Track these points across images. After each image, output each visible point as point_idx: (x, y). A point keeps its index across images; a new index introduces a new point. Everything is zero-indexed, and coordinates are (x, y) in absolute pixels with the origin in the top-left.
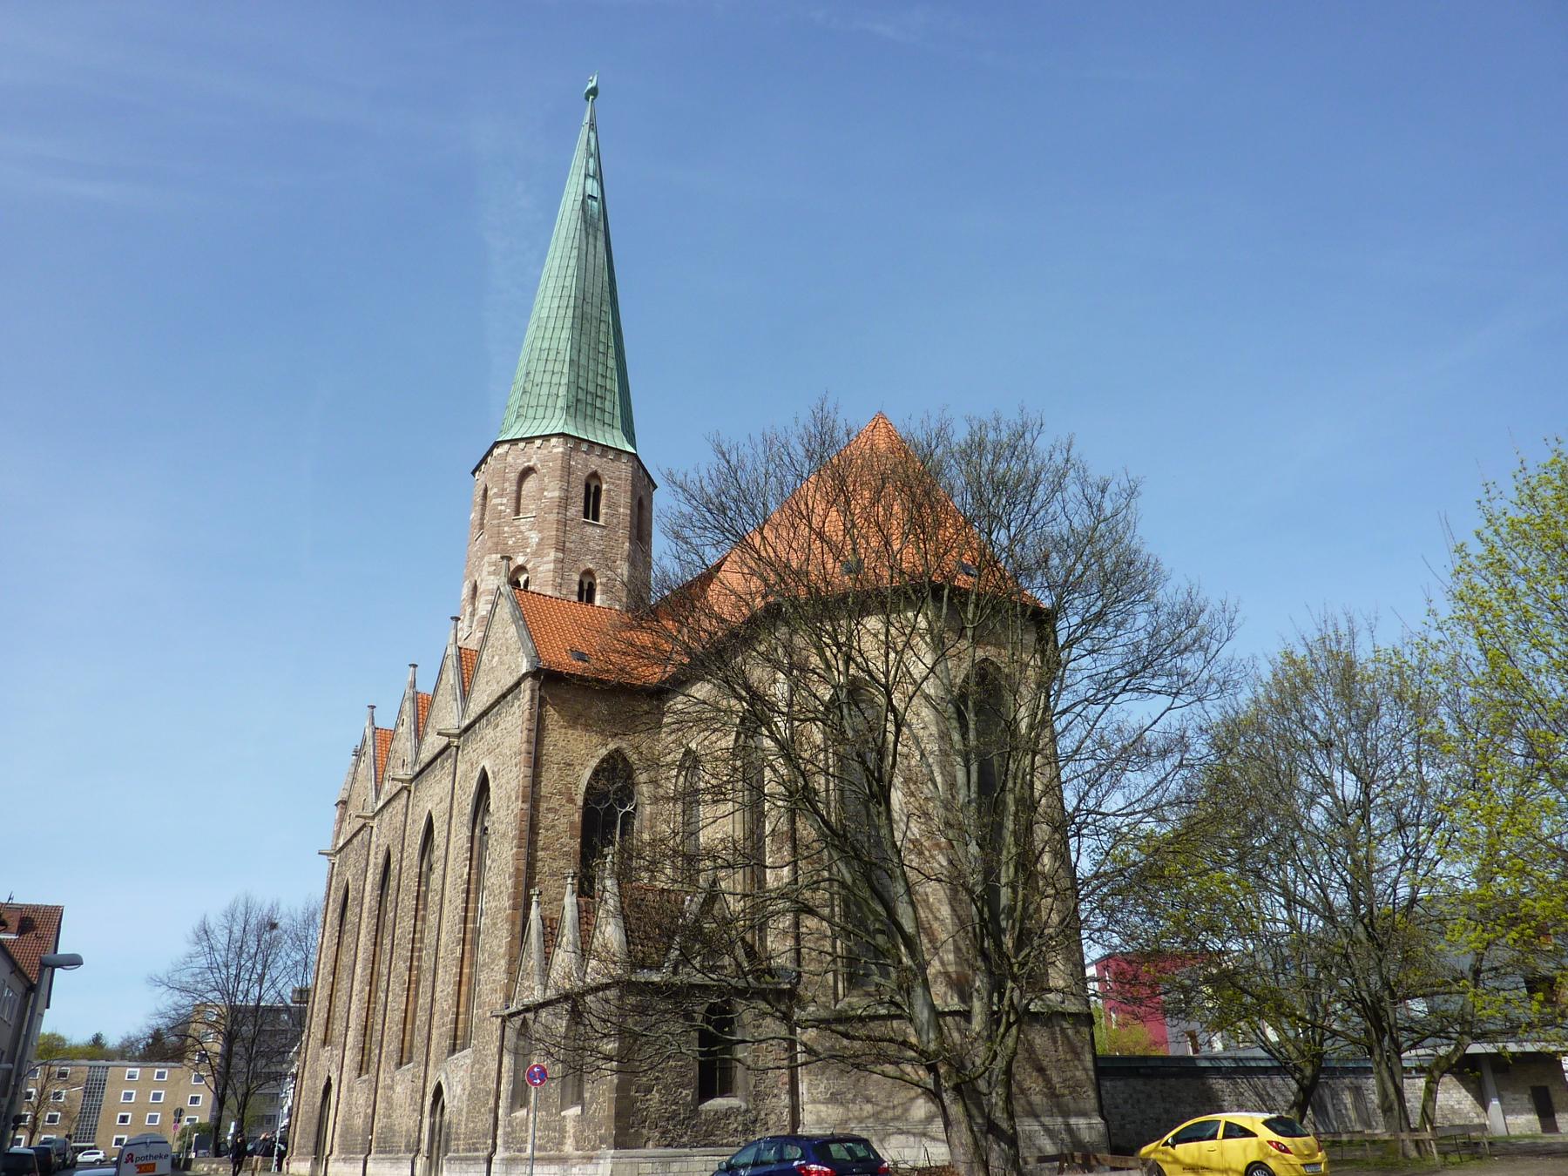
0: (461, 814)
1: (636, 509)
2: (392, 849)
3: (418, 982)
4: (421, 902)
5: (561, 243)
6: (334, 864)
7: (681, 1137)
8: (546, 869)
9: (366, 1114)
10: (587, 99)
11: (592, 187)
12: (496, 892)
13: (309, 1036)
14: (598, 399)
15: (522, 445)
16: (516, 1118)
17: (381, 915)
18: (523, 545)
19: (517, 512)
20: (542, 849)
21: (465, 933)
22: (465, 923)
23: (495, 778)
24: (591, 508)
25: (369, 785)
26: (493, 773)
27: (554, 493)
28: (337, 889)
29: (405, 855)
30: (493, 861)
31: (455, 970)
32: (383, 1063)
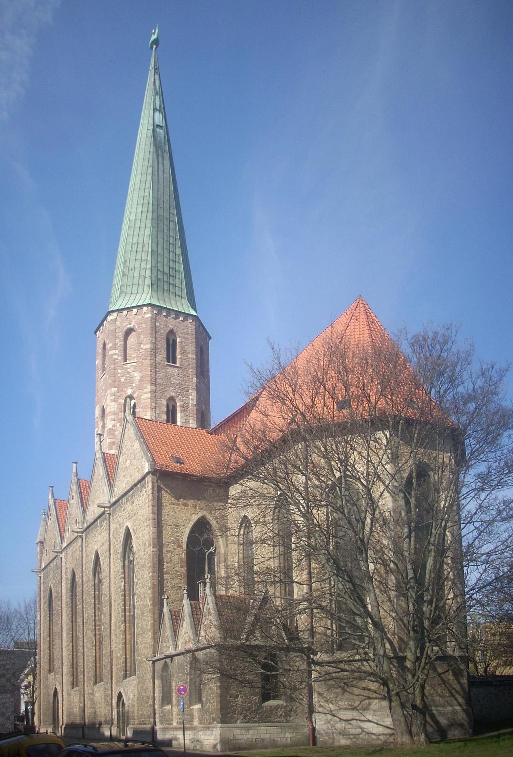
0: (116, 552)
1: (199, 355)
2: (75, 571)
3: (101, 643)
4: (97, 600)
5: (141, 164)
6: (40, 577)
7: (254, 718)
8: (169, 584)
9: (80, 707)
10: (152, 48)
11: (159, 118)
12: (142, 597)
13: (40, 667)
14: (171, 278)
15: (125, 313)
16: (165, 709)
17: (74, 606)
18: (130, 381)
19: (125, 359)
20: (166, 573)
21: (125, 618)
22: (125, 612)
23: (135, 533)
24: (171, 357)
25: (56, 533)
26: (133, 530)
27: (147, 346)
28: (45, 591)
29: (84, 574)
30: (138, 580)
31: (122, 637)
32: (86, 682)
